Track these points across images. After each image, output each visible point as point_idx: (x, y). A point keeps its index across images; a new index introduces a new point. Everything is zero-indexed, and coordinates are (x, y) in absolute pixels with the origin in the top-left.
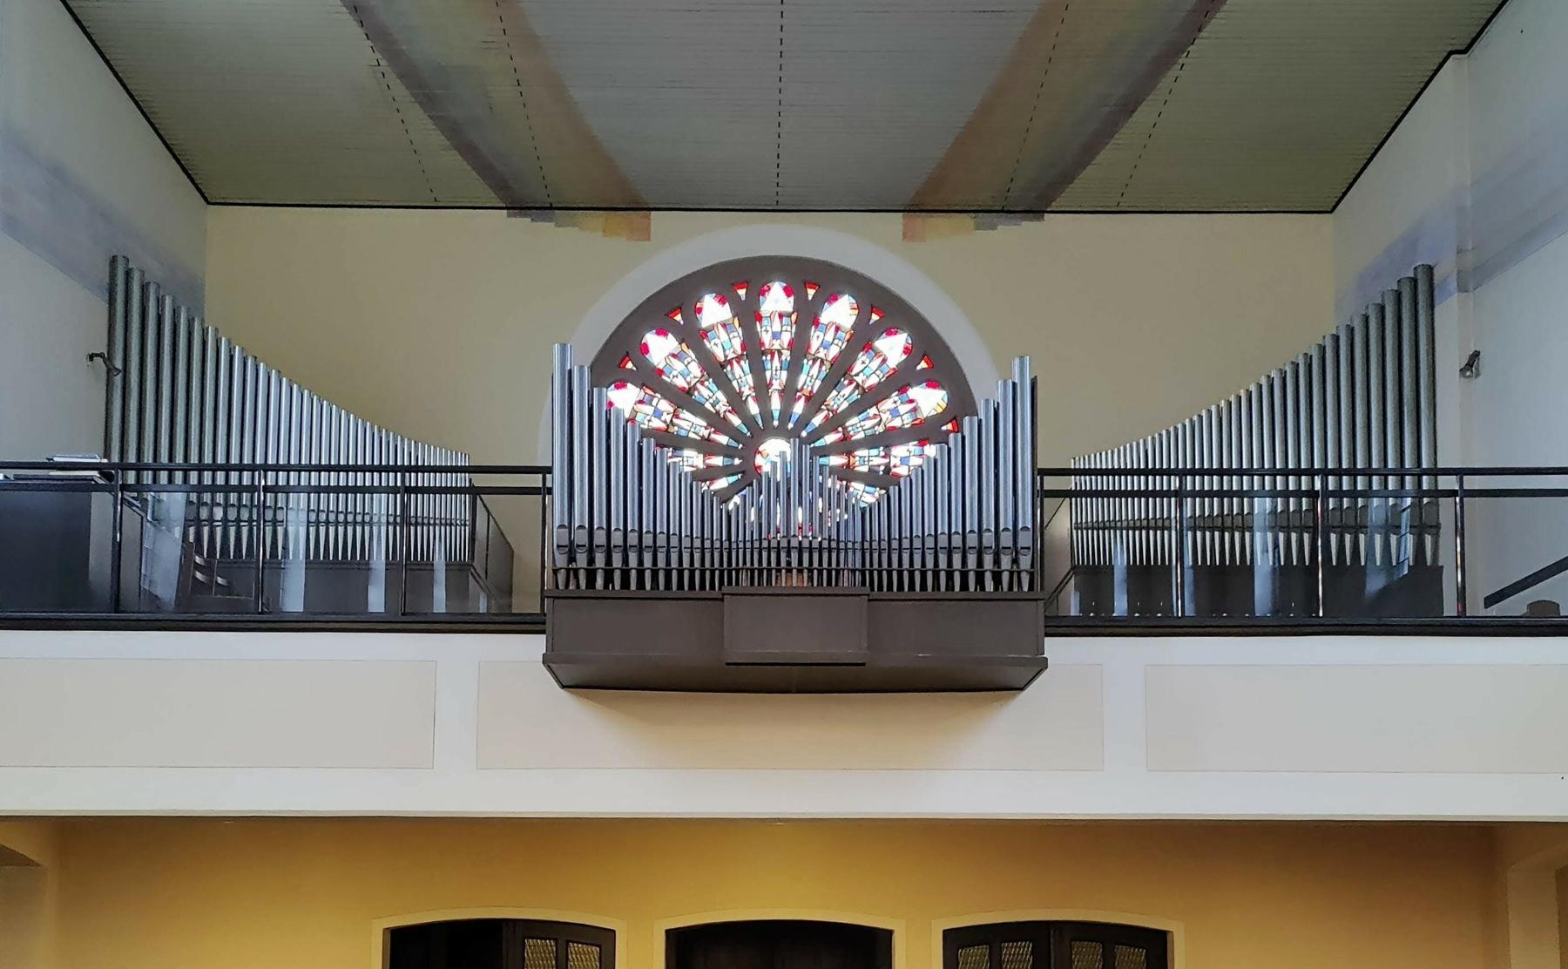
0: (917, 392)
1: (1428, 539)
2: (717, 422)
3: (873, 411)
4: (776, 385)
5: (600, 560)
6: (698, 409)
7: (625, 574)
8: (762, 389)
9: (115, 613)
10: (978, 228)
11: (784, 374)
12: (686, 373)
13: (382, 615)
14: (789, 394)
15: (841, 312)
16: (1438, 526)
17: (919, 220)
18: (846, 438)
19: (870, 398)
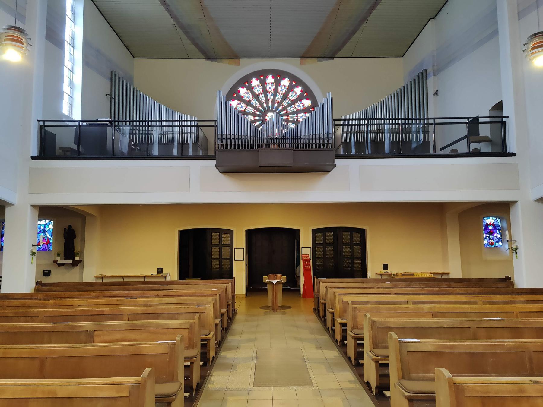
1: (426, 135)
2: (256, 109)
3: (293, 106)
5: (229, 142)
6: (252, 106)
7: (235, 145)
8: (267, 101)
11: (272, 97)
14: (273, 102)
15: (286, 82)
16: (429, 132)
17: (304, 60)
19: (293, 102)
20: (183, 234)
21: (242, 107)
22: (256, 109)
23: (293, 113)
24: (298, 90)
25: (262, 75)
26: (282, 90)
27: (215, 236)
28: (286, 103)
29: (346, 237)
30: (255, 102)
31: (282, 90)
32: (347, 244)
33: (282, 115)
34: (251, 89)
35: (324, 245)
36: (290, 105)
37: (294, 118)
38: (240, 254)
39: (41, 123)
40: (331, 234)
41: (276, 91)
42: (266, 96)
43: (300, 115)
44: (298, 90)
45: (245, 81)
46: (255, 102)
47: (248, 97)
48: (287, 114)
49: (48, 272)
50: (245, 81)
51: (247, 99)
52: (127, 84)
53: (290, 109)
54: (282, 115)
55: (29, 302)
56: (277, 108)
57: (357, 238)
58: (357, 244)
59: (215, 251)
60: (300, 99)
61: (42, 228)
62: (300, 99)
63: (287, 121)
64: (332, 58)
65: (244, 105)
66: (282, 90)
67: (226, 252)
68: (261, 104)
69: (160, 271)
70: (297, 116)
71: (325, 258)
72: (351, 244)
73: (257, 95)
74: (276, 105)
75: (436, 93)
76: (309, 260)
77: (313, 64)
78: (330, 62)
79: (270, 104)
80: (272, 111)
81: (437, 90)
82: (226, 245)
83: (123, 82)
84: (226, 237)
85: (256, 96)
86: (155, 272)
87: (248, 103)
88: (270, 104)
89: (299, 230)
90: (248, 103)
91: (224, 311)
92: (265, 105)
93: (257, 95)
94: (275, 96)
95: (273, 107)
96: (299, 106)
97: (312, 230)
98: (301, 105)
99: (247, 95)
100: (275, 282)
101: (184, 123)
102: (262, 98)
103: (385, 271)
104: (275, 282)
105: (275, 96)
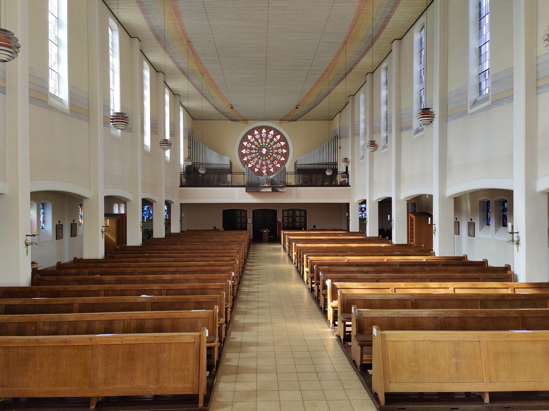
0: (281, 143)
1: (336, 166)
2: (257, 146)
3: (276, 145)
4: (264, 142)
5: (250, 183)
6: (254, 145)
7: (252, 184)
8: (262, 142)
9: (104, 296)
10: (289, 122)
11: (265, 140)
12: (253, 140)
13: (205, 335)
14: (266, 143)
15: (272, 132)
16: (337, 164)
17: (281, 121)
18: (268, 143)
19: (275, 143)
24: (278, 137)
25: (259, 129)
27: (238, 212)
29: (298, 213)
32: (298, 217)
35: (288, 217)
37: (276, 151)
39: (181, 173)
44: (278, 137)
49: (389, 219)
52: (196, 141)
58: (303, 217)
59: (239, 220)
64: (296, 120)
66: (270, 137)
67: (243, 219)
68: (259, 144)
70: (278, 150)
71: (288, 223)
72: (300, 217)
75: (340, 148)
77: (286, 124)
78: (295, 122)
81: (340, 147)
82: (244, 217)
83: (194, 139)
86: (213, 229)
91: (249, 241)
98: (280, 145)
100: (265, 231)
101: (220, 173)
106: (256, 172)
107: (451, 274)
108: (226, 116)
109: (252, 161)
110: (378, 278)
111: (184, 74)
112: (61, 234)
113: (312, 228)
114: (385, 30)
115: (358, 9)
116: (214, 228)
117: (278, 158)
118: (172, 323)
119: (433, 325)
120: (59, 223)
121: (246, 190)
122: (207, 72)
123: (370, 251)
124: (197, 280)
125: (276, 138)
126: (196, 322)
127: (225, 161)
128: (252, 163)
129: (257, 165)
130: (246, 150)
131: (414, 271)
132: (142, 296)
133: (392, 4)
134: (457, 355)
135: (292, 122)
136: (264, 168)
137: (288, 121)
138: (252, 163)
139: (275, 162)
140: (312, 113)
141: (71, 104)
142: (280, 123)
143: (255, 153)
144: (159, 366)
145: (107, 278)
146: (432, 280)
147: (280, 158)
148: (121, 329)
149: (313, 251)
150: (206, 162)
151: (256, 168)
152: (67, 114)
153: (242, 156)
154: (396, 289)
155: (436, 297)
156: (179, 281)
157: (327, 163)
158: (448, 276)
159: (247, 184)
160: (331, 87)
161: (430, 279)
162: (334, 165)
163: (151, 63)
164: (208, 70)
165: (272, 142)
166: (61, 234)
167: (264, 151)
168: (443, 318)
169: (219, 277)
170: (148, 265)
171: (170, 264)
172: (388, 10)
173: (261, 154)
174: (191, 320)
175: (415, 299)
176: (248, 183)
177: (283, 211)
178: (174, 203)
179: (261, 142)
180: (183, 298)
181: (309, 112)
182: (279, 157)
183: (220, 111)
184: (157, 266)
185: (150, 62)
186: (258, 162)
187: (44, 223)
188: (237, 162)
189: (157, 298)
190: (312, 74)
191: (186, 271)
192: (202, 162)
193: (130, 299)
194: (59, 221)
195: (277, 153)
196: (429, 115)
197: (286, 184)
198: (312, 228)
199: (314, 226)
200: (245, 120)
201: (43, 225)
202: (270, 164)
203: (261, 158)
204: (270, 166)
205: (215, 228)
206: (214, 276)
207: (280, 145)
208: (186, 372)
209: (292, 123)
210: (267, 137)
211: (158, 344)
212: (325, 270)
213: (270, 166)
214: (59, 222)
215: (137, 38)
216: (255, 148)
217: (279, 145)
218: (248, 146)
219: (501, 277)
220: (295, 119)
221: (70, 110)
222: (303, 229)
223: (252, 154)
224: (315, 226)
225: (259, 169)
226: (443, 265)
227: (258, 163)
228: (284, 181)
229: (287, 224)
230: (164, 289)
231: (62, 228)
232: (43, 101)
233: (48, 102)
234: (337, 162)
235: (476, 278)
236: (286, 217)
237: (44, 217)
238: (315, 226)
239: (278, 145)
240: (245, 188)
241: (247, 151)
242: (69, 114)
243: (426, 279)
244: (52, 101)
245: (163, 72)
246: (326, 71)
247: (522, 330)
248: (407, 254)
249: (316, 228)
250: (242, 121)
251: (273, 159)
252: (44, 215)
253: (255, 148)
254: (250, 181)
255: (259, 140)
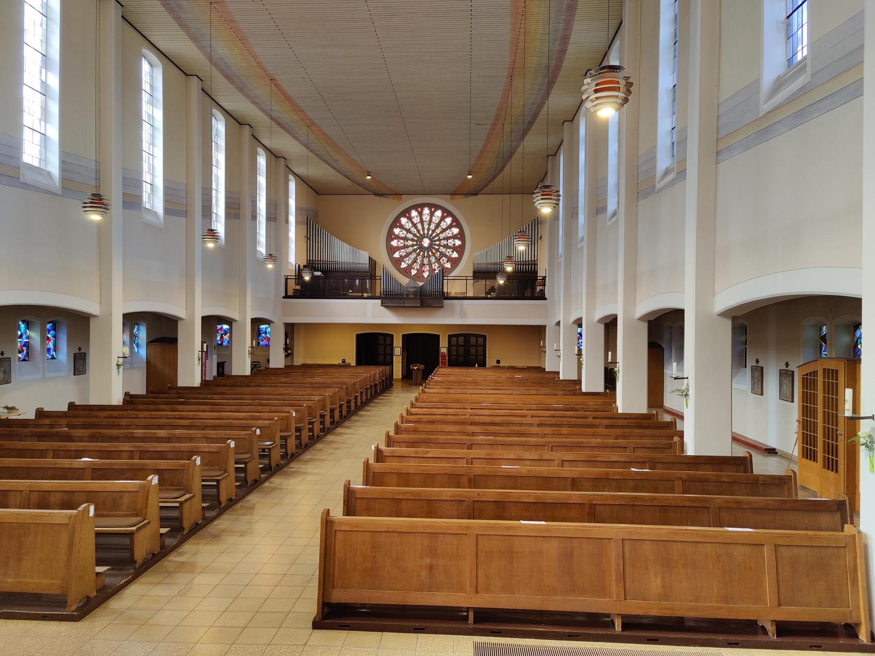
2: (415, 235)
3: (444, 233)
7: (388, 295)
8: (423, 229)
9: (53, 459)
11: (428, 226)
14: (428, 229)
17: (453, 196)
19: (444, 230)
20: (358, 336)
21: (403, 234)
22: (415, 235)
23: (444, 239)
26: (436, 219)
27: (381, 337)
28: (438, 231)
29: (473, 340)
30: (413, 230)
31: (436, 219)
33: (436, 241)
34: (410, 219)
35: (458, 345)
36: (441, 232)
37: (445, 243)
38: (398, 351)
40: (462, 338)
41: (430, 221)
42: (423, 225)
43: (450, 241)
45: (406, 213)
46: (413, 230)
47: (408, 225)
48: (439, 240)
50: (406, 213)
51: (408, 228)
52: (318, 227)
53: (442, 236)
54: (436, 241)
55: (115, 413)
56: (431, 235)
57: (480, 340)
59: (381, 348)
60: (450, 227)
61: (264, 330)
62: (450, 227)
63: (439, 245)
64: (476, 194)
65: (405, 232)
68: (418, 231)
69: (344, 361)
71: (458, 355)
72: (477, 346)
73: (416, 224)
74: (430, 232)
75: (541, 238)
76: (445, 356)
77: (459, 199)
78: (475, 197)
79: (426, 232)
80: (427, 237)
81: (542, 236)
84: (388, 339)
85: (414, 225)
86: (341, 362)
87: (408, 231)
88: (426, 232)
89: (439, 336)
90: (408, 231)
92: (422, 233)
93: (416, 224)
94: (429, 224)
95: (428, 234)
96: (449, 233)
97: (449, 335)
98: (450, 233)
99: (407, 224)
100: (415, 368)
101: (363, 278)
102: (419, 226)
103: (498, 365)
104: (415, 368)
105: (429, 224)
106: (414, 275)
107: (583, 440)
108: (365, 188)
109: (406, 257)
110: (469, 443)
111: (281, 128)
112: (83, 367)
113: (495, 364)
114: (567, 56)
115: (512, 26)
116: (343, 362)
117: (447, 254)
118: (87, 497)
119: (456, 512)
120: (80, 351)
121: (382, 303)
122: (314, 124)
123: (524, 402)
124: (205, 439)
125: (445, 221)
126: (121, 498)
127: (362, 259)
128: (407, 261)
129: (415, 265)
130: (399, 241)
131: (544, 434)
132: (83, 459)
133: (563, 17)
134: (432, 552)
135: (469, 198)
136: (426, 269)
137: (462, 196)
138: (407, 261)
139: (443, 260)
140: (497, 182)
141: (64, 179)
142: (451, 199)
143: (413, 246)
144: (21, 554)
145: (77, 432)
146: (554, 448)
147: (450, 253)
148: (18, 504)
149: (436, 400)
150: (331, 260)
151: (414, 269)
152: (55, 194)
153: (391, 250)
154: (474, 460)
155: (506, 472)
156: (179, 439)
157: (531, 260)
158: (578, 443)
159: (384, 294)
160: (514, 144)
161: (550, 446)
162: (526, 264)
163: (227, 112)
164: (315, 121)
165: (438, 228)
166: (83, 367)
167: (426, 242)
168: (472, 502)
169: (236, 435)
170: (163, 415)
171: (195, 415)
172: (561, 26)
173: (421, 248)
174: (115, 494)
175: (474, 475)
176: (385, 293)
177: (450, 337)
178: (274, 323)
179: (422, 228)
180: (136, 464)
181: (492, 181)
182: (449, 252)
183: (354, 182)
184: (177, 417)
185: (226, 111)
186: (417, 260)
187: (55, 351)
188: (383, 260)
189: (101, 463)
190: (476, 124)
191: (205, 426)
192: (326, 260)
193: (63, 463)
194: (80, 348)
195: (446, 247)
196: (551, 196)
197: (446, 295)
198: (495, 364)
199: (498, 362)
200: (397, 194)
201: (54, 353)
202: (435, 263)
203: (422, 253)
204: (435, 266)
205: (344, 361)
206: (229, 434)
207: (450, 233)
208: (54, 564)
209: (470, 198)
210: (430, 221)
211: (21, 525)
212: (409, 428)
213: (435, 266)
214: (80, 349)
215: (196, 75)
216: (413, 239)
217: (449, 233)
218: (402, 235)
219: (660, 446)
220: (474, 193)
221: (62, 188)
222: (477, 366)
223: (408, 247)
224: (499, 361)
225: (418, 271)
226: (605, 425)
227: (416, 262)
228: (441, 290)
229: (482, 357)
230: (138, 451)
231: (85, 359)
232: (9, 176)
233: (19, 178)
234: (537, 260)
235: (621, 447)
236: (455, 346)
237: (55, 341)
238: (499, 361)
239: (449, 233)
240: (379, 301)
241: (400, 243)
242: (60, 192)
243: (544, 447)
244: (27, 177)
245: (249, 125)
246: (497, 118)
247: (588, 522)
248: (573, 408)
249: (501, 365)
250: (392, 196)
251: (440, 255)
252: (55, 338)
253: (412, 237)
254: (387, 290)
255: (419, 225)
